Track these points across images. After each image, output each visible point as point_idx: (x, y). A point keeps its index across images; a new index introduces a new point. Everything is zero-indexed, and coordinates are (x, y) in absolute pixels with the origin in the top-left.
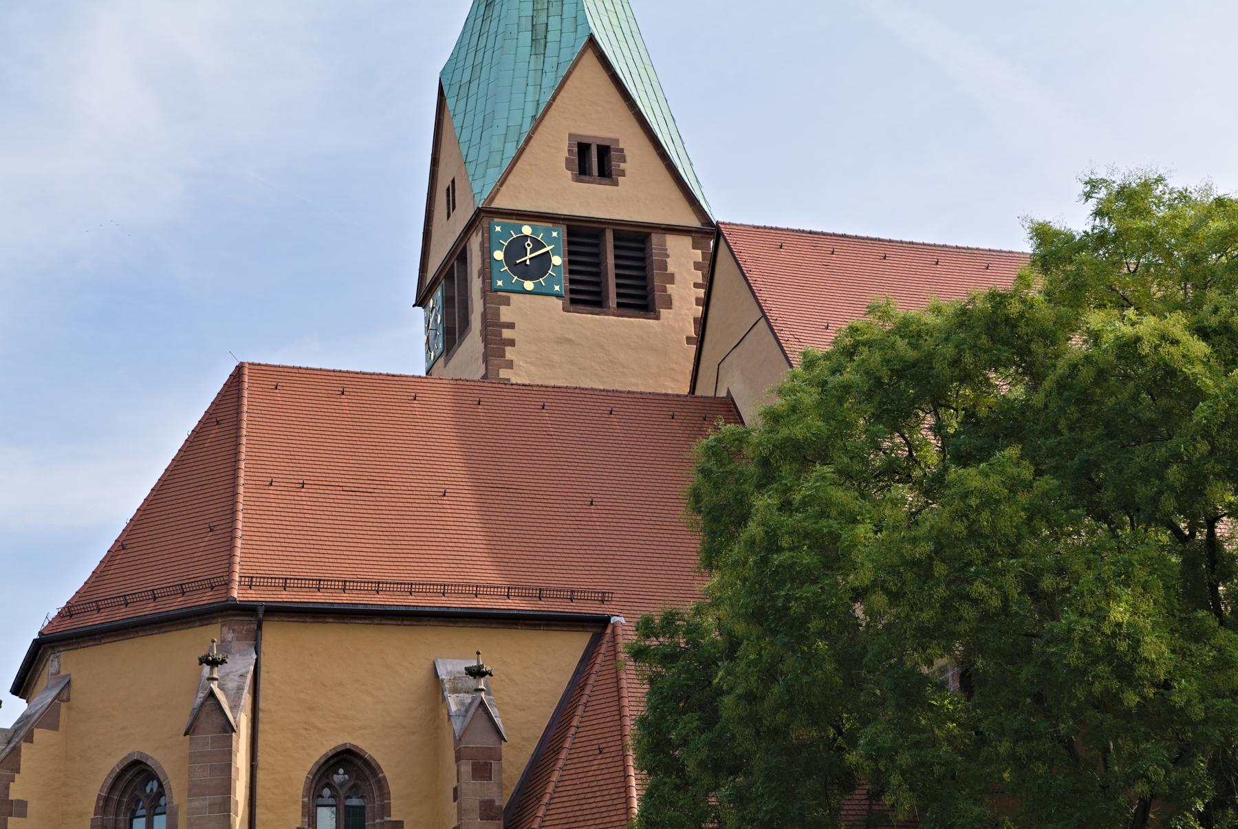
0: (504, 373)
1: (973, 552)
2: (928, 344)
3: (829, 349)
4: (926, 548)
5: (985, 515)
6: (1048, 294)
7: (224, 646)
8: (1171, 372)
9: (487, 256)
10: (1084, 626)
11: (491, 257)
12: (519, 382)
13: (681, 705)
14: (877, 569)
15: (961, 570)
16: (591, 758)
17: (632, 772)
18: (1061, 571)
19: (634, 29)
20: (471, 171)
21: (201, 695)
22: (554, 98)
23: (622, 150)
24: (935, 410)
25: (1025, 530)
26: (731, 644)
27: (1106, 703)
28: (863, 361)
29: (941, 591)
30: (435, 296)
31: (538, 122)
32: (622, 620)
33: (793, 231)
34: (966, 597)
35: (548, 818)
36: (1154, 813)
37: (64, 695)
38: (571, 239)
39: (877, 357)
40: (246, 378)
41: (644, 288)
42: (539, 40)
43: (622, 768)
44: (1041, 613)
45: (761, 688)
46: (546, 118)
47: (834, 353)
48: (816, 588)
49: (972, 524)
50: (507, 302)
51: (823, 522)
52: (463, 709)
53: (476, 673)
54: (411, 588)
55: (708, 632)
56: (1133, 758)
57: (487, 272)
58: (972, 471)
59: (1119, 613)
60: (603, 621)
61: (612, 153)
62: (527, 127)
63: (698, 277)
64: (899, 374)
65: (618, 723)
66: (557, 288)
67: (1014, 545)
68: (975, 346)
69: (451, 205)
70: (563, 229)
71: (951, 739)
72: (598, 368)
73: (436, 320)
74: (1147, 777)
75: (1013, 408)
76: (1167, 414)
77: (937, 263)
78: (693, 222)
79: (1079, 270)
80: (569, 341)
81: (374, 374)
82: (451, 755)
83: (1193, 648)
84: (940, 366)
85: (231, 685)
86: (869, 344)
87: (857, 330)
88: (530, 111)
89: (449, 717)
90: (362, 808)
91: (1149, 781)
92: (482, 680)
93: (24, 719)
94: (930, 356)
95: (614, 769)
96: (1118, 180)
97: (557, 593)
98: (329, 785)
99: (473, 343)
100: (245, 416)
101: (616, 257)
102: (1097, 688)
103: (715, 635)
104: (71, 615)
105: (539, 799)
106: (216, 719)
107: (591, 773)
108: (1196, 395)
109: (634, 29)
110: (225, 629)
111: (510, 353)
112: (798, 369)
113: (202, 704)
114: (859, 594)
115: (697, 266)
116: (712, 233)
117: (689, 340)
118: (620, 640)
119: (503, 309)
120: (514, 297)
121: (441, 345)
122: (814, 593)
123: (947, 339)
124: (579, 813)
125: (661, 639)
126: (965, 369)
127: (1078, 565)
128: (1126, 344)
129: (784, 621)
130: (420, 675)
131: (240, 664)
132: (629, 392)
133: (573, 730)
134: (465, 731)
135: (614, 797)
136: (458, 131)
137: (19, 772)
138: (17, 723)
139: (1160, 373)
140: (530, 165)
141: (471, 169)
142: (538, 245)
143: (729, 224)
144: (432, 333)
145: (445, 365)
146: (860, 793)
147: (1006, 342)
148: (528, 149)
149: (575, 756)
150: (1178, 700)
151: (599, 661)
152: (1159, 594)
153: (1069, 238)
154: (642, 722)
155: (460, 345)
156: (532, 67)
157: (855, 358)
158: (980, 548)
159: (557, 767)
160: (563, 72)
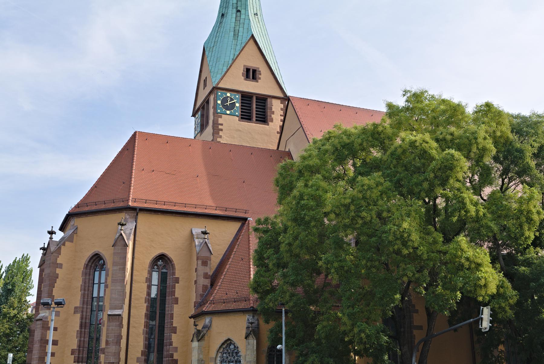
0: (218, 140)
1: (363, 203)
2: (352, 138)
3: (321, 138)
4: (348, 201)
5: (369, 192)
6: (391, 125)
7: (126, 220)
8: (425, 152)
9: (215, 102)
10: (394, 228)
11: (217, 102)
12: (223, 142)
13: (268, 246)
14: (333, 206)
15: (358, 208)
16: (239, 261)
17: (252, 266)
18: (389, 211)
19: (266, 33)
20: (212, 75)
21: (118, 235)
22: (239, 54)
23: (260, 71)
24: (353, 159)
25: (379, 198)
26: (285, 228)
27: (398, 252)
28: (332, 142)
29: (353, 214)
30: (198, 114)
31: (234, 61)
32: (251, 219)
33: (312, 100)
34: (360, 217)
35: (224, 279)
36: (411, 287)
37: (75, 232)
38: (242, 98)
39: (337, 141)
40: (137, 136)
41: (264, 115)
42: (236, 35)
43: (248, 265)
44: (381, 223)
45: (293, 242)
46: (237, 59)
47: (323, 139)
48: (314, 212)
49: (364, 194)
50: (221, 117)
51: (317, 192)
52: (200, 244)
53: (205, 233)
54: (185, 205)
55: (278, 224)
56: (404, 269)
57: (215, 107)
58: (365, 178)
59: (405, 225)
60: (245, 219)
61: (257, 72)
62: (230, 62)
63: (282, 113)
64: (343, 147)
65: (248, 251)
66: (237, 114)
67: (375, 202)
68: (367, 140)
69: (205, 85)
70: (240, 95)
71: (351, 261)
72: (248, 139)
73: (198, 121)
74: (407, 275)
75: (377, 160)
76: (424, 164)
77: (357, 113)
78: (281, 95)
79: (400, 118)
80: (240, 130)
81: (177, 137)
82: (195, 258)
83: (427, 237)
84: (356, 146)
85: (127, 232)
86: (334, 137)
87: (330, 133)
88: (232, 57)
89: (195, 246)
90: (167, 273)
91: (408, 277)
92: (206, 235)
93: (63, 239)
94: (353, 142)
95: (246, 265)
96: (413, 91)
97: (231, 210)
98: (157, 265)
99: (209, 129)
100: (136, 148)
101: (256, 105)
102: (396, 247)
103: (280, 225)
104: (79, 207)
105: (222, 273)
106: (122, 242)
107: (239, 266)
108: (432, 159)
109: (266, 33)
110: (126, 215)
111: (221, 133)
112: (311, 144)
113: (118, 237)
114: (326, 214)
115: (282, 109)
116: (287, 99)
117: (278, 132)
118: (250, 225)
119: (220, 119)
120: (223, 116)
121: (199, 129)
122: (313, 214)
123: (359, 137)
124: (234, 278)
125: (263, 226)
126: (364, 147)
127: (394, 210)
128: (412, 142)
129: (303, 222)
130: (187, 233)
131: (131, 226)
132: (258, 148)
133: (234, 253)
134: (200, 251)
135: (246, 274)
136: (209, 62)
137: (60, 255)
138: (60, 239)
139: (422, 152)
140: (231, 74)
141: (212, 74)
142: (232, 100)
143: (293, 97)
144: (197, 125)
145: (200, 136)
146: (322, 276)
147: (377, 139)
148: (230, 69)
149: (234, 260)
150: (419, 253)
151: (243, 232)
152: (418, 221)
153: (398, 107)
154: (256, 251)
155: (205, 130)
156: (233, 43)
157: (330, 141)
158: (365, 202)
159: (228, 264)
160: (243, 45)
